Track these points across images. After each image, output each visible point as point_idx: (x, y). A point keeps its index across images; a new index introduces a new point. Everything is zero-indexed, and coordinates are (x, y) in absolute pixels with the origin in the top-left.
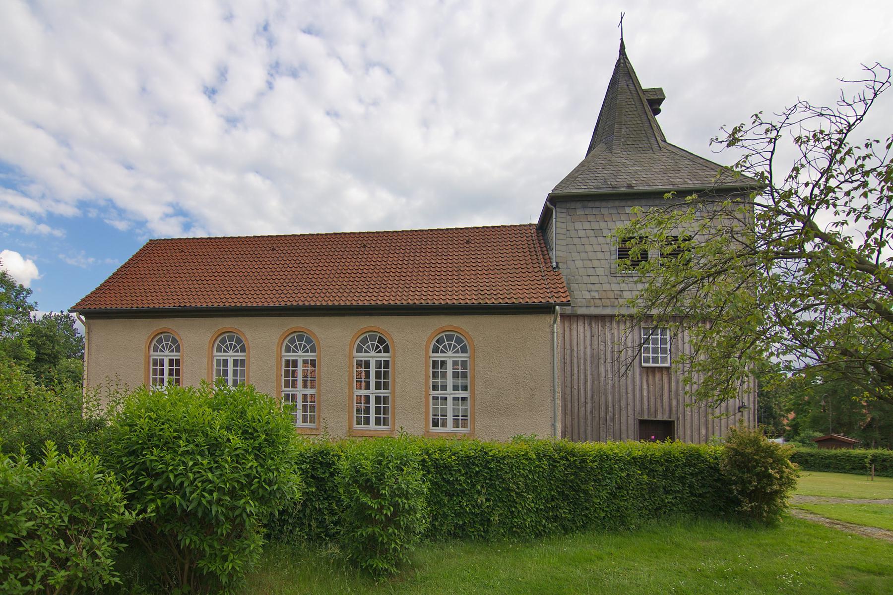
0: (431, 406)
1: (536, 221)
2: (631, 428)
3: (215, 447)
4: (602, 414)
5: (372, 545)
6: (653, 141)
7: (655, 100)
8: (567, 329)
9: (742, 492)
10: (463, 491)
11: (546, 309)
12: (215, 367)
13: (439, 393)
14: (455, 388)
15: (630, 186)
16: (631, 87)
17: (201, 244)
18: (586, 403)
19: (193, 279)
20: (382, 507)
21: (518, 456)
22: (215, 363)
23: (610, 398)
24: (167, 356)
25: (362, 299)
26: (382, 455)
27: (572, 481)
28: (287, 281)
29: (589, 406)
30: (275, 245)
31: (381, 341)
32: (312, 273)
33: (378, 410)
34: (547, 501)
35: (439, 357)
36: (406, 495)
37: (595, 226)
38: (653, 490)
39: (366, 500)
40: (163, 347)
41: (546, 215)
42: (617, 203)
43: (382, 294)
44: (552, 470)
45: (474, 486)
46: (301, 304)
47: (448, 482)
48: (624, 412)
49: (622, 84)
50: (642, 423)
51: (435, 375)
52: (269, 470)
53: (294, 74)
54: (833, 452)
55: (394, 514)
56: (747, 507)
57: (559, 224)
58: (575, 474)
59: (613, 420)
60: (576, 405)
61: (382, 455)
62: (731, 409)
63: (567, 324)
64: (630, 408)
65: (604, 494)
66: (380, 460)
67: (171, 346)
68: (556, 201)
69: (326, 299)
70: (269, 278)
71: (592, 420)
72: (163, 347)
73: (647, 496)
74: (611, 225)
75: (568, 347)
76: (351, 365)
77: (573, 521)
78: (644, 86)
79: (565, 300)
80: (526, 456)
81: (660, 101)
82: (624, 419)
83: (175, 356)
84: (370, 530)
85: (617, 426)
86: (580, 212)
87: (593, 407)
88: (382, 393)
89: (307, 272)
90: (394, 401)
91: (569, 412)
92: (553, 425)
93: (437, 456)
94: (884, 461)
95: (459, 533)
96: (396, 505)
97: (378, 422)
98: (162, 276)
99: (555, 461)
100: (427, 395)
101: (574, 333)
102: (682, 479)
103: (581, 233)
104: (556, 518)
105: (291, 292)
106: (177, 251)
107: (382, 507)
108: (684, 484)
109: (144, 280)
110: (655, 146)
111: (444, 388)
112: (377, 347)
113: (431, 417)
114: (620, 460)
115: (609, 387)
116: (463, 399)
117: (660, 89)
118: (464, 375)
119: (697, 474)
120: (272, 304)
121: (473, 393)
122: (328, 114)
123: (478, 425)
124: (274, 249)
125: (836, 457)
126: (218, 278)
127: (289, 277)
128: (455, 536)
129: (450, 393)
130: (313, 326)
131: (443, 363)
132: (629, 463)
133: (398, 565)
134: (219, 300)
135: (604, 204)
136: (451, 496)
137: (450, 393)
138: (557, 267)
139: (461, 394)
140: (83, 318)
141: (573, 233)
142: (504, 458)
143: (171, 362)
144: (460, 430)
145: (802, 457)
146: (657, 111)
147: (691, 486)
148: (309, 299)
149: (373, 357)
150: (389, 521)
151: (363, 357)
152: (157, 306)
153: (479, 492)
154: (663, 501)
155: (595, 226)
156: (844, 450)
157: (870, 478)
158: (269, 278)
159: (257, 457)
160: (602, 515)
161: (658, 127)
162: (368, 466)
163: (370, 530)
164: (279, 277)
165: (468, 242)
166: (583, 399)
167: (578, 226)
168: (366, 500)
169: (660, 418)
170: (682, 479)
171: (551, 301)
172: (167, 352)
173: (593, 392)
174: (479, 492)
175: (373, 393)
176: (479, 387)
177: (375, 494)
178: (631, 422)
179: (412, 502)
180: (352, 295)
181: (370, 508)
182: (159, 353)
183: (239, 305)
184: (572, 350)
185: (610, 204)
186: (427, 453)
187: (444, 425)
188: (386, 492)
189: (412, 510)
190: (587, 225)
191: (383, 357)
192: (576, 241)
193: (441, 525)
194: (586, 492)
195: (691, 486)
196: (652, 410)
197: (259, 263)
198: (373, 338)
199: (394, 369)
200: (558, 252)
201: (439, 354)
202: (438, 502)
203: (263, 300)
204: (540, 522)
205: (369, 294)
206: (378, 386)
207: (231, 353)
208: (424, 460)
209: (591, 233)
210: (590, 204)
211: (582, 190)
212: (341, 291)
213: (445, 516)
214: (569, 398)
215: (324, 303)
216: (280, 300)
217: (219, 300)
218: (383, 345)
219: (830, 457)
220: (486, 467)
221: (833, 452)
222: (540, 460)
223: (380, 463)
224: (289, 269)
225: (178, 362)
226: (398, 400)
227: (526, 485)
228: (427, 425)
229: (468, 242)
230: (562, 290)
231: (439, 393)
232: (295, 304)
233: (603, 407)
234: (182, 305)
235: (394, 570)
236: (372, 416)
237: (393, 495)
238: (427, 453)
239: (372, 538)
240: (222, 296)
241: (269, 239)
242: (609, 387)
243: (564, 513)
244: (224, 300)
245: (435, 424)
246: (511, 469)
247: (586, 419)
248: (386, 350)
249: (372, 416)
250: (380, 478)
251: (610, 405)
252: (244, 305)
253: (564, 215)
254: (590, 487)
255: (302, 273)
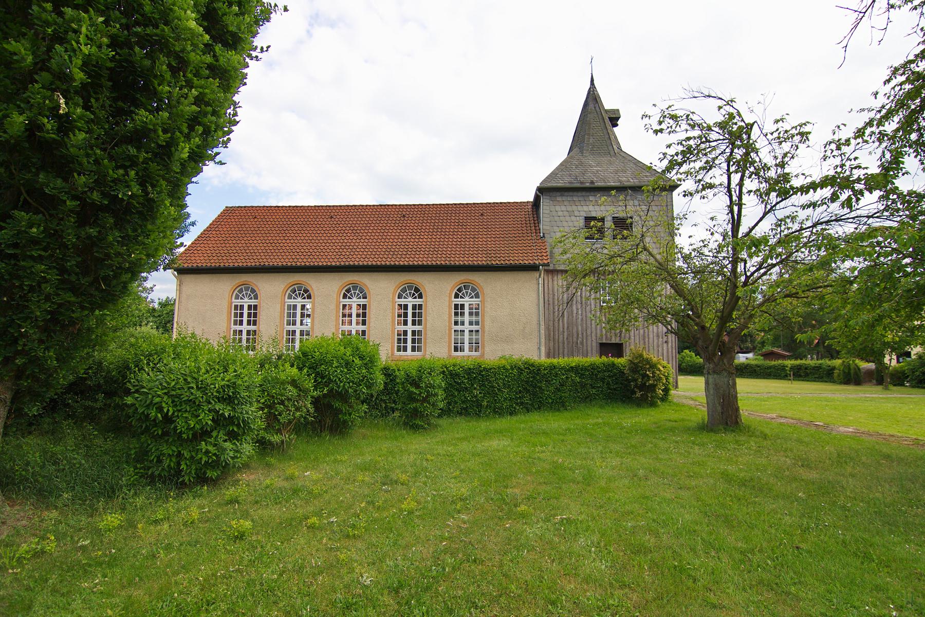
0: (453, 337)
1: (531, 199)
2: (594, 348)
3: (348, 364)
4: (575, 339)
5: (415, 413)
6: (610, 148)
7: (614, 119)
8: (550, 280)
9: (636, 386)
10: (466, 388)
11: (533, 268)
12: (286, 311)
13: (459, 328)
14: (471, 323)
15: (592, 182)
16: (597, 108)
17: (271, 211)
18: (563, 332)
19: (268, 242)
20: (421, 393)
21: (499, 368)
22: (286, 308)
23: (580, 329)
24: (246, 302)
25: (403, 260)
26: (421, 367)
27: (532, 382)
28: (344, 244)
29: (566, 334)
30: (332, 214)
31: (417, 290)
32: (364, 238)
33: (413, 341)
34: (516, 393)
35: (459, 301)
36: (433, 387)
37: (569, 208)
38: (583, 386)
39: (413, 390)
40: (243, 295)
41: (537, 198)
42: (584, 193)
43: (417, 256)
44: (520, 376)
45: (473, 385)
46: (356, 263)
47: (458, 383)
48: (589, 338)
49: (591, 106)
50: (602, 345)
51: (456, 314)
52: (371, 374)
53: (332, 24)
54: (773, 363)
55: (427, 397)
56: (638, 395)
57: (545, 206)
58: (533, 377)
59: (582, 343)
60: (556, 333)
61: (421, 367)
62: (660, 334)
63: (550, 277)
64: (593, 335)
65: (552, 389)
66: (420, 370)
67: (250, 295)
68: (542, 191)
69: (375, 260)
70: (329, 241)
71: (568, 344)
72: (243, 295)
73: (579, 390)
74: (580, 208)
75: (551, 292)
76: (394, 308)
77: (532, 405)
78: (607, 107)
79: (546, 262)
80: (504, 367)
81: (618, 118)
82: (589, 343)
83: (253, 302)
84: (414, 405)
85: (585, 348)
86: (559, 199)
87: (568, 335)
88: (417, 328)
89: (359, 238)
90: (426, 334)
91: (552, 339)
92: (539, 348)
93: (451, 368)
94: (806, 369)
95: (464, 412)
96: (428, 392)
97: (413, 349)
98: (241, 239)
99: (522, 370)
100: (450, 329)
101: (555, 283)
102: (603, 380)
103: (560, 213)
104: (522, 403)
105: (348, 253)
106: (251, 217)
107: (421, 393)
108: (604, 383)
109: (226, 242)
110: (612, 152)
111: (463, 323)
112: (414, 294)
113: (453, 345)
114: (562, 368)
115: (579, 320)
116: (478, 331)
117: (618, 110)
118: (477, 314)
119: (612, 376)
120: (334, 264)
121: (483, 327)
122: (366, 61)
123: (487, 349)
124: (332, 217)
125: (774, 367)
126: (288, 241)
127: (346, 241)
128: (461, 414)
129: (467, 327)
130: (365, 280)
131: (462, 306)
132: (568, 370)
133: (428, 424)
134: (291, 260)
135: (575, 193)
136: (459, 391)
137: (467, 327)
138: (544, 236)
139: (474, 328)
140: (176, 273)
141: (554, 213)
142: (491, 369)
143: (250, 307)
144: (474, 353)
145: (752, 368)
146: (616, 125)
147: (608, 384)
148: (362, 260)
149: (410, 302)
150: (425, 400)
151: (403, 301)
152: (241, 265)
153: (475, 389)
154: (589, 393)
155: (569, 208)
156: (780, 362)
157: (790, 382)
158: (329, 241)
159: (366, 368)
160: (550, 401)
161: (616, 137)
162: (414, 373)
163: (414, 405)
164: (337, 241)
165: (482, 215)
166: (561, 330)
167: (558, 208)
168: (413, 390)
169: (613, 341)
170: (603, 380)
171: (537, 262)
172: (246, 300)
173: (568, 324)
174: (475, 389)
175: (410, 328)
176: (488, 323)
177: (418, 387)
178: (594, 344)
179: (436, 391)
180: (395, 256)
181: (416, 393)
182: (239, 300)
183: (307, 264)
184: (554, 295)
185: (580, 194)
186: (446, 367)
187: (462, 350)
188: (423, 385)
189: (436, 395)
190: (563, 208)
191: (418, 301)
192: (557, 218)
193: (453, 408)
194: (540, 388)
195: (608, 384)
196: (599, 335)
197: (320, 229)
198: (410, 288)
199: (426, 311)
200: (545, 225)
201: (459, 299)
202: (452, 395)
203: (326, 260)
204: (512, 406)
205: (408, 256)
206: (414, 323)
207: (299, 299)
208: (444, 371)
209: (566, 213)
210: (566, 194)
211: (560, 184)
212: (387, 253)
213: (456, 403)
214: (552, 328)
215: (374, 263)
216: (340, 260)
217: (291, 260)
218: (418, 292)
219: (770, 367)
220: (480, 374)
221: (773, 363)
222: (512, 369)
223: (420, 371)
224: (345, 235)
225: (256, 307)
226: (429, 333)
227: (504, 384)
228: (449, 350)
229: (482, 215)
230: (545, 254)
231: (459, 328)
232: (351, 263)
233: (575, 336)
234: (262, 264)
235: (426, 426)
236: (409, 345)
237: (427, 387)
238: (446, 367)
239: (415, 409)
240: (294, 257)
241: (328, 208)
242: (579, 320)
243: (526, 400)
244: (295, 260)
245: (456, 349)
246: (495, 375)
247: (563, 343)
248: (420, 296)
249: (409, 345)
250: (420, 378)
251: (580, 333)
252: (312, 264)
253: (548, 201)
254: (543, 385)
255: (355, 238)
